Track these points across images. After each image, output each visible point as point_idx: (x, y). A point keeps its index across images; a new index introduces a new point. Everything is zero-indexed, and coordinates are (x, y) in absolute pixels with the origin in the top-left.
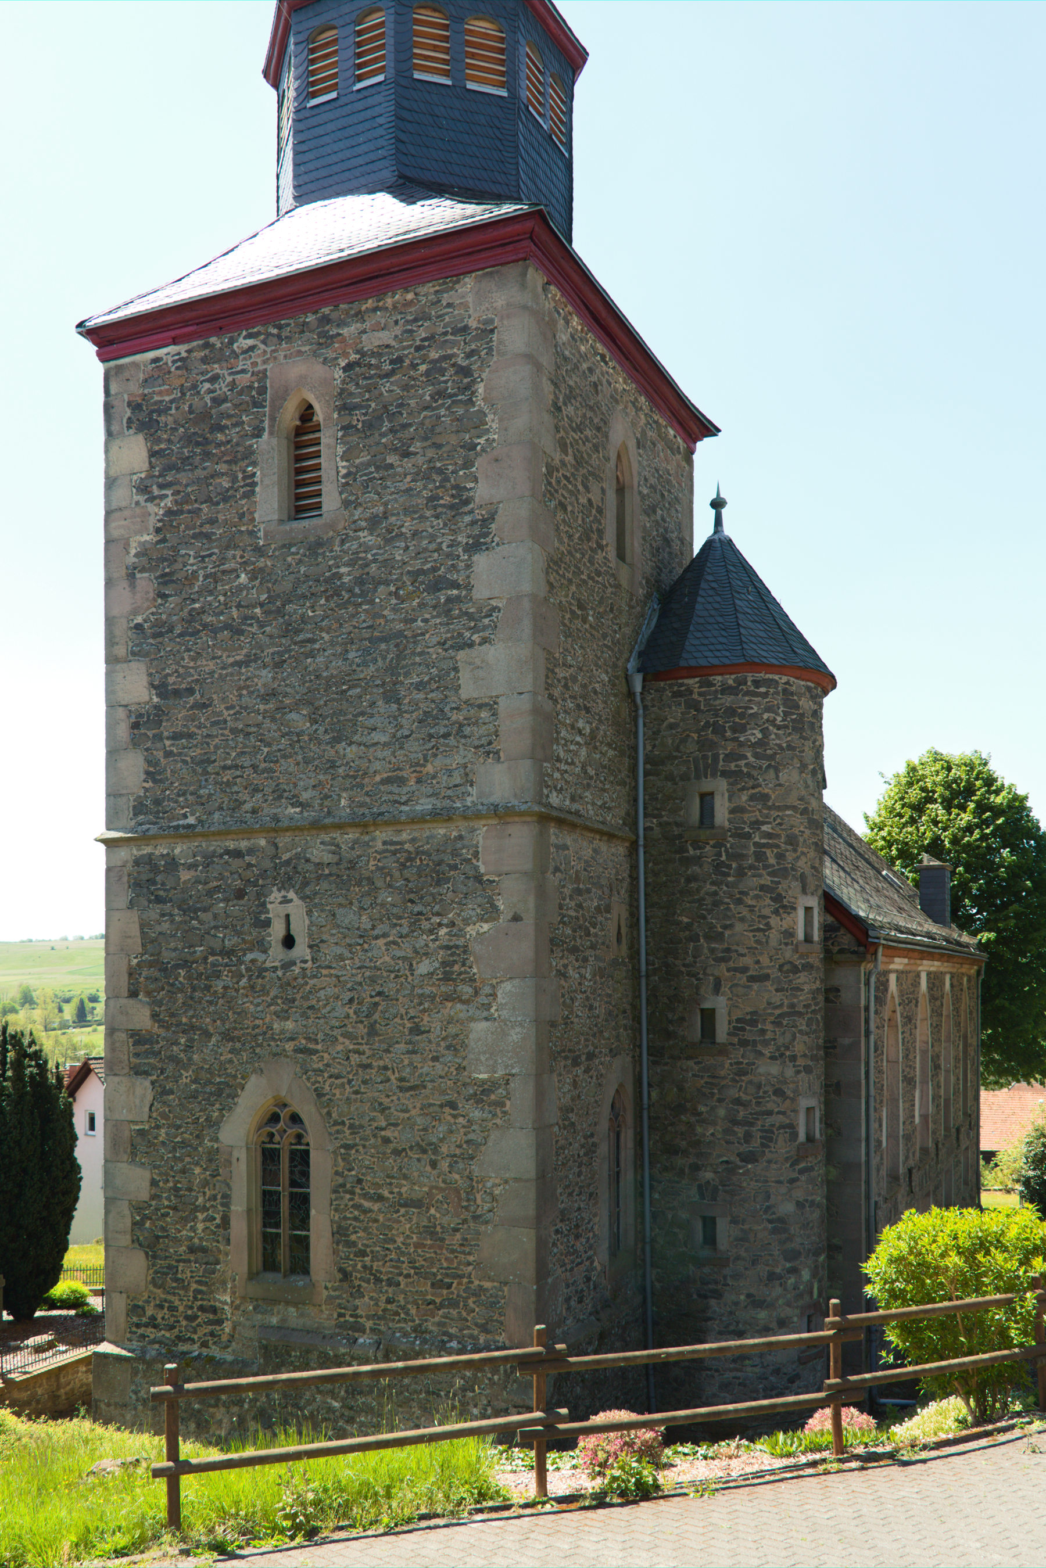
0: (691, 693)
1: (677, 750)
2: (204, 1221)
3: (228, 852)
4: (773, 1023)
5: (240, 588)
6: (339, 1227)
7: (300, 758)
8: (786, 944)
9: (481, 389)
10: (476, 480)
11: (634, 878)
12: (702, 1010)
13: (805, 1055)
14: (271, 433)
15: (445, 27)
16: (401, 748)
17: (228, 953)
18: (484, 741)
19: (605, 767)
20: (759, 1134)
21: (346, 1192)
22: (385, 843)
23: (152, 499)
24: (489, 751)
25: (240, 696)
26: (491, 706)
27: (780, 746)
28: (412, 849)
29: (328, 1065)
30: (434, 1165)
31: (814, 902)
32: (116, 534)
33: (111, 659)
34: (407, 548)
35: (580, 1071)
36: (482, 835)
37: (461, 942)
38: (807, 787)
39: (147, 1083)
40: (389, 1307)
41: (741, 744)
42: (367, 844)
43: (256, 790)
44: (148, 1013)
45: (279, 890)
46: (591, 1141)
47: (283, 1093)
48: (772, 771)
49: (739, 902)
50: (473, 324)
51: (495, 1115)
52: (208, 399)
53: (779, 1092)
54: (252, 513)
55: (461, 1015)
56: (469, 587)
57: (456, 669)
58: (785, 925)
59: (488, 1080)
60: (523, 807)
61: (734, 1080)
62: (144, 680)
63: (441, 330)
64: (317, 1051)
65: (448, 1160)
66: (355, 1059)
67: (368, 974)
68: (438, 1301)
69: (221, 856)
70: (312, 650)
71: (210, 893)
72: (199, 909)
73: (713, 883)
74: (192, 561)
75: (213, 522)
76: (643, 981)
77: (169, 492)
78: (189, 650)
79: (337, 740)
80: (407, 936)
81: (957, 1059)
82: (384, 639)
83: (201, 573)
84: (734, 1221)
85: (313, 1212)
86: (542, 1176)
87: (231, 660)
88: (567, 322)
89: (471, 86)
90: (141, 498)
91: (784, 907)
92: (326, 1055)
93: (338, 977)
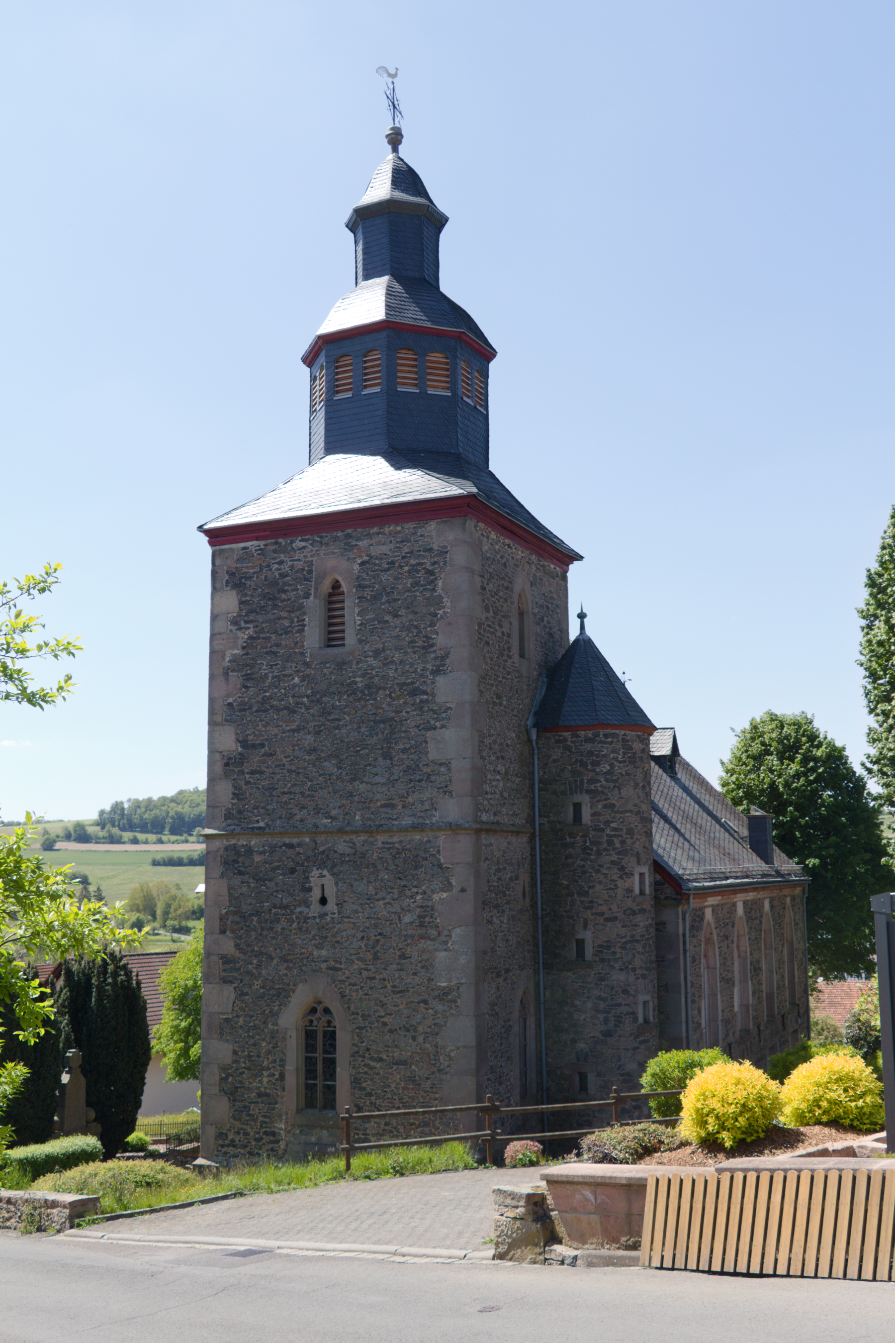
0: (567, 741)
1: (559, 776)
2: (268, 1076)
3: (285, 845)
4: (620, 947)
5: (295, 686)
6: (355, 1079)
7: (331, 789)
8: (628, 897)
9: (440, 583)
10: (437, 633)
11: (533, 855)
12: (577, 940)
13: (641, 968)
14: (315, 597)
15: (415, 360)
16: (393, 787)
17: (286, 907)
18: (443, 785)
19: (513, 790)
20: (614, 1019)
21: (360, 1056)
22: (383, 843)
23: (240, 629)
24: (446, 790)
25: (294, 750)
26: (447, 765)
27: (621, 774)
28: (400, 847)
29: (348, 978)
30: (414, 1038)
31: (645, 869)
32: (217, 648)
33: (212, 723)
34: (396, 669)
35: (501, 980)
36: (442, 840)
37: (430, 904)
38: (639, 797)
39: (231, 988)
40: (386, 1128)
41: (597, 774)
42: (372, 843)
43: (303, 808)
44: (232, 944)
45: (317, 869)
46: (508, 1024)
47: (320, 995)
48: (616, 789)
49: (598, 871)
50: (435, 547)
51: (451, 1008)
52: (276, 574)
53: (625, 992)
54: (303, 642)
55: (430, 948)
56: (433, 695)
57: (426, 742)
58: (627, 885)
59: (447, 987)
60: (467, 825)
61: (596, 984)
62: (233, 737)
63: (417, 549)
64: (341, 969)
65: (423, 1036)
66: (365, 974)
67: (373, 922)
68: (417, 1123)
69: (281, 847)
70: (339, 725)
71: (274, 870)
72: (267, 880)
73: (582, 860)
74: (264, 667)
75: (278, 645)
76: (540, 921)
77: (251, 626)
78: (262, 721)
79: (353, 780)
80: (397, 899)
81: (780, 962)
82: (383, 722)
83: (271, 675)
84: (599, 1075)
85: (338, 1069)
86: (479, 1045)
87: (288, 728)
88: (488, 537)
89: (430, 391)
90: (234, 628)
91: (626, 874)
92: (347, 972)
93: (354, 923)
